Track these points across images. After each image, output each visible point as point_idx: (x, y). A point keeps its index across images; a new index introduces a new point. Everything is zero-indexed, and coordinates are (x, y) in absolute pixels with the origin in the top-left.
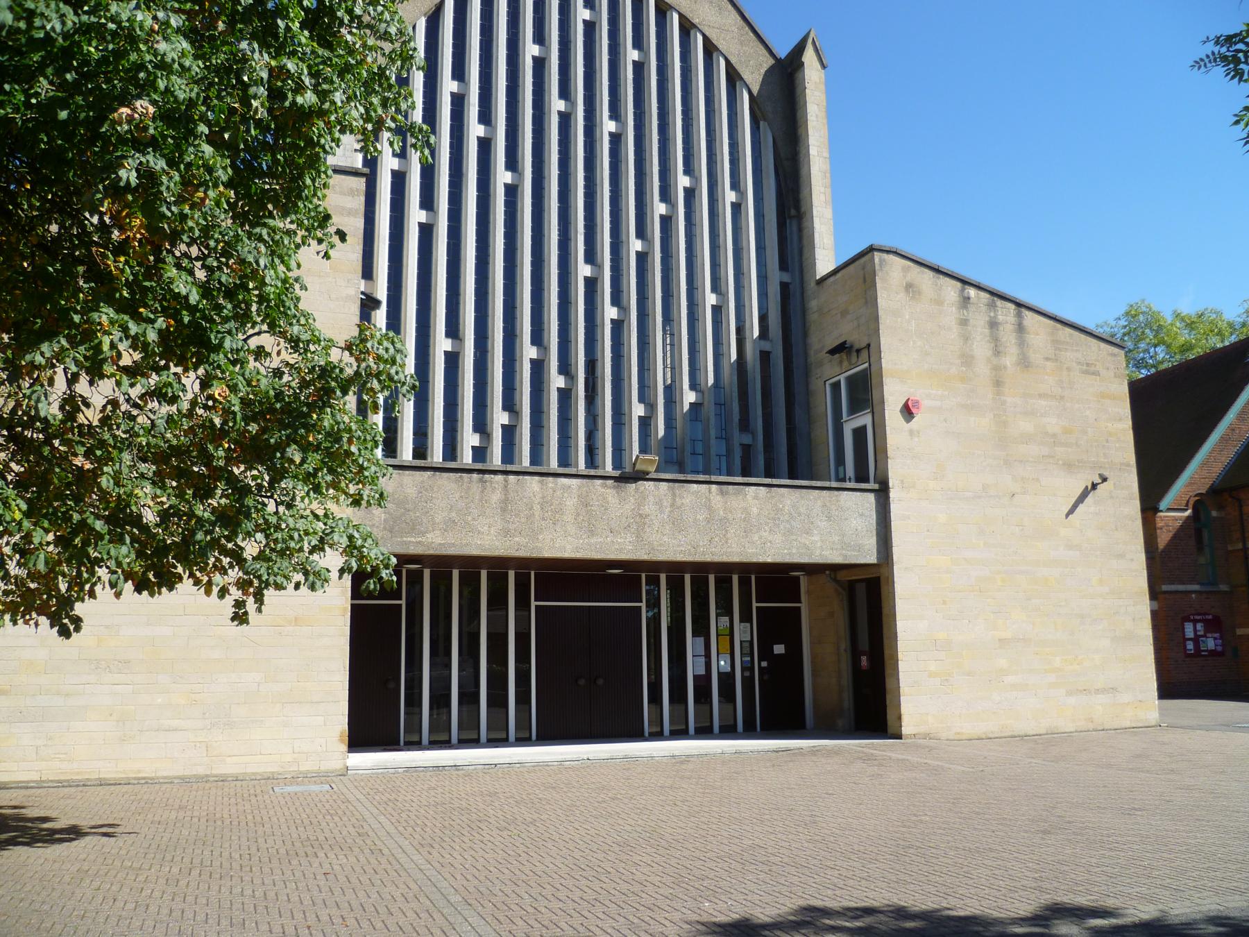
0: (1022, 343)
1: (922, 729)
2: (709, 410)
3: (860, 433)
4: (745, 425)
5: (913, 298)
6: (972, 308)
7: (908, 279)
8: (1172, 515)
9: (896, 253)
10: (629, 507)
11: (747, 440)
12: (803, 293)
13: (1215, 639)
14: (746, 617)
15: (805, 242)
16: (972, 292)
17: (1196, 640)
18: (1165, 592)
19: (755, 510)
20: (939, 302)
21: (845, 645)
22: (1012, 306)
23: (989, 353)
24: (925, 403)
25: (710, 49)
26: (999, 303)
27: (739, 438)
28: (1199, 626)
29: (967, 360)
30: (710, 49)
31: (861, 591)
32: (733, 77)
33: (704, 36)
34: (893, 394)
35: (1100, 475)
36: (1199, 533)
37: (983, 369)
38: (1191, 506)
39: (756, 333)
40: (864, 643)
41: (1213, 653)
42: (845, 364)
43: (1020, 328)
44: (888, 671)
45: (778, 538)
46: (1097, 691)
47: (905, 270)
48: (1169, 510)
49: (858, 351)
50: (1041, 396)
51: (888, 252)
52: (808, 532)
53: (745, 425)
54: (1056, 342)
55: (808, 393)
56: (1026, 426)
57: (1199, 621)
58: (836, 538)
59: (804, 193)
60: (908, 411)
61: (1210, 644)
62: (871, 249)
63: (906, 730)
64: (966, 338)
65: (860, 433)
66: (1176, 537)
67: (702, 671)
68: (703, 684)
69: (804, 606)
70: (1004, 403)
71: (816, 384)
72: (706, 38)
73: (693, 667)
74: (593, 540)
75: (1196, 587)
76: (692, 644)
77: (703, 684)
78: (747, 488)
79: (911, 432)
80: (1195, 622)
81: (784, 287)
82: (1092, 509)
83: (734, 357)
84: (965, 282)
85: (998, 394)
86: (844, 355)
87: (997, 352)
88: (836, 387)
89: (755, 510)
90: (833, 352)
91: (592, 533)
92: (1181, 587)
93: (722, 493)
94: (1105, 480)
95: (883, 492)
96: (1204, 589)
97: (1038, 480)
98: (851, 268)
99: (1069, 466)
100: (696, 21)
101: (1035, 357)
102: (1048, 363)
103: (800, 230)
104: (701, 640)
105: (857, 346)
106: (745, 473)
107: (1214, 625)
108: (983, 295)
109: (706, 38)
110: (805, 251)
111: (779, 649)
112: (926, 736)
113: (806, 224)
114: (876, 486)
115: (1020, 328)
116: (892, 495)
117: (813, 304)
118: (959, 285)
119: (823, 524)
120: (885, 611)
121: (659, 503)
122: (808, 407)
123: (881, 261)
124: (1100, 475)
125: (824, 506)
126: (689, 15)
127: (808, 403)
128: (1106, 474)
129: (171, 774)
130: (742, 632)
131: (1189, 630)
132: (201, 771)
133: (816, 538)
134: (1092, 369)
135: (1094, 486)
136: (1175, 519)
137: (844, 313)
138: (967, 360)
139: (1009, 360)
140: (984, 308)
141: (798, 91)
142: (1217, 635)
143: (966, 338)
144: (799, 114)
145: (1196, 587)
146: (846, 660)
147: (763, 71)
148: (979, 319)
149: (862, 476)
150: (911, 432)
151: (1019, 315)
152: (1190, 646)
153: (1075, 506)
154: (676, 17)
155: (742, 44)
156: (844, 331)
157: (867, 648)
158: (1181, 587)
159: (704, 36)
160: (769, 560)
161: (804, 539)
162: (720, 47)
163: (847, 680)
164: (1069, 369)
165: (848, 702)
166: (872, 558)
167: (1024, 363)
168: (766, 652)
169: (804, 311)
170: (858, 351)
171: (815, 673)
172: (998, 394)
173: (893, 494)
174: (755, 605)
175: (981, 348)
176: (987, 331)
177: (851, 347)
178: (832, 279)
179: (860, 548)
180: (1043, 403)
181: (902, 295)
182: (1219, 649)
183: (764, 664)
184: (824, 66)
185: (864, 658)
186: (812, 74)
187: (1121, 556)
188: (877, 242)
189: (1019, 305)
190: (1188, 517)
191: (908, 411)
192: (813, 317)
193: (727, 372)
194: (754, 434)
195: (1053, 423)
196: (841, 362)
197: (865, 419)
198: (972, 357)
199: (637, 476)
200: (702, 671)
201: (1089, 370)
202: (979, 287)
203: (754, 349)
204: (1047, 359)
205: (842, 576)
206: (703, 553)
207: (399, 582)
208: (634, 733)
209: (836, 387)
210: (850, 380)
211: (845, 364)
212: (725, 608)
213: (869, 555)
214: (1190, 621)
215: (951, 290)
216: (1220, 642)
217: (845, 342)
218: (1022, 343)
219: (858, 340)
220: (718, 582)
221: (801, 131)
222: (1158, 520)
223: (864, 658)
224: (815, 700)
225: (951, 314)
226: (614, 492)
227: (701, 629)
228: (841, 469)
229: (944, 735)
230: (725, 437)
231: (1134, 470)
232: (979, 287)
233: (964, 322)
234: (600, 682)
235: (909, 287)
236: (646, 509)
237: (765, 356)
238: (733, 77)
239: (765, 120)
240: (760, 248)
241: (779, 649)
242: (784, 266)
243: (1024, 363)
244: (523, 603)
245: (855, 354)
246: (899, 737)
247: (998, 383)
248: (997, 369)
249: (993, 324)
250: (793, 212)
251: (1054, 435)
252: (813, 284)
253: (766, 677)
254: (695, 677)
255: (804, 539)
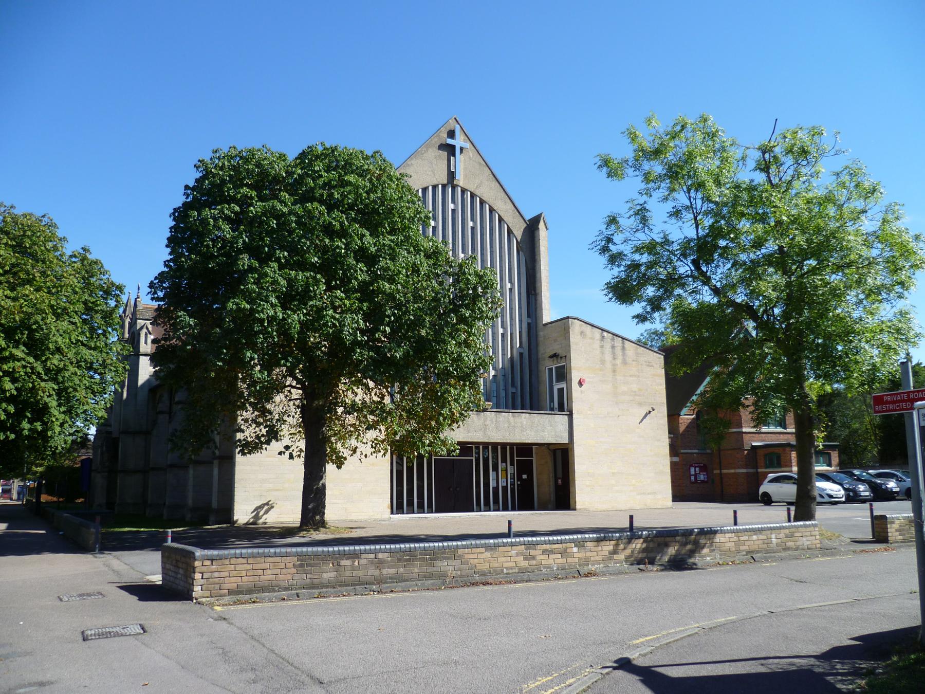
0: (624, 354)
1: (583, 507)
2: (500, 378)
3: (561, 391)
4: (513, 385)
5: (583, 338)
6: (605, 341)
7: (582, 330)
8: (686, 416)
9: (577, 319)
10: (481, 421)
11: (514, 390)
12: (536, 328)
13: (704, 475)
14: (512, 464)
15: (538, 305)
16: (605, 334)
17: (695, 475)
18: (682, 453)
19: (525, 423)
20: (593, 339)
21: (552, 475)
22: (621, 339)
23: (611, 359)
24: (587, 380)
25: (501, 220)
26: (616, 338)
27: (511, 390)
28: (697, 469)
29: (603, 362)
30: (501, 220)
31: (559, 454)
32: (510, 232)
33: (499, 215)
34: (575, 376)
35: (652, 408)
36: (698, 426)
37: (609, 366)
38: (695, 413)
39: (518, 346)
40: (560, 474)
41: (703, 482)
42: (555, 362)
43: (623, 348)
44: (571, 484)
45: (533, 433)
46: (648, 494)
47: (581, 326)
48: (685, 415)
49: (561, 358)
50: (630, 376)
51: (574, 319)
52: (543, 431)
53: (513, 385)
54: (637, 354)
55: (538, 371)
56: (624, 388)
57: (697, 467)
58: (553, 433)
59: (538, 285)
60: (580, 383)
61: (702, 477)
62: (568, 318)
63: (577, 507)
64: (603, 353)
65: (561, 391)
66: (688, 427)
67: (505, 485)
68: (496, 490)
69: (534, 459)
70: (616, 379)
71: (542, 368)
72: (499, 216)
73: (492, 484)
74: (469, 434)
75: (696, 451)
76: (492, 475)
77: (496, 490)
78: (522, 414)
79: (581, 392)
80: (695, 467)
81: (529, 324)
82: (649, 421)
83: (509, 356)
84: (603, 330)
85: (614, 375)
86: (555, 358)
87: (614, 359)
88: (551, 370)
89: (525, 423)
90: (551, 357)
91: (469, 432)
92: (690, 451)
93: (513, 416)
94: (654, 410)
95: (570, 415)
96: (700, 452)
97: (628, 410)
98: (559, 323)
99: (640, 404)
100: (495, 208)
101: (629, 360)
102: (634, 362)
103: (536, 300)
104: (495, 472)
105: (561, 355)
106: (522, 409)
107: (704, 468)
108: (610, 335)
109: (499, 216)
110: (538, 309)
111: (525, 477)
112: (585, 509)
113: (538, 298)
114: (568, 413)
115: (623, 348)
116: (574, 417)
117: (541, 334)
118: (601, 331)
119: (549, 428)
120: (570, 461)
121: (491, 420)
122: (538, 377)
123: (572, 323)
124: (652, 408)
125: (549, 421)
126: (493, 206)
127: (538, 375)
128: (654, 407)
129: (335, 519)
130: (510, 470)
131: (692, 471)
132: (344, 518)
133: (546, 433)
134: (651, 364)
135: (650, 412)
136: (688, 419)
137: (555, 341)
138: (603, 362)
139: (619, 361)
140: (610, 341)
141: (536, 239)
142: (705, 473)
143: (603, 353)
144: (536, 250)
145: (696, 451)
146: (552, 483)
147: (522, 230)
148: (608, 346)
149: (561, 408)
150: (581, 392)
151: (623, 343)
152: (693, 478)
153: (642, 420)
154: (487, 206)
155: (514, 218)
156: (555, 348)
157: (561, 476)
158: (690, 451)
159: (499, 215)
160: (530, 442)
161: (542, 434)
162: (505, 219)
163: (552, 488)
164: (641, 365)
165: (553, 497)
166: (566, 442)
167: (625, 362)
168: (520, 478)
169: (537, 336)
170: (561, 358)
171: (538, 486)
172: (614, 375)
173: (574, 416)
174: (516, 458)
175: (608, 357)
176: (611, 350)
177: (558, 355)
178: (550, 325)
179: (561, 437)
180: (631, 378)
181: (579, 336)
182: (706, 479)
183: (519, 483)
184: (547, 229)
185: (560, 480)
186: (542, 232)
187: (659, 440)
188: (570, 315)
189: (623, 339)
190: (693, 418)
191: (580, 383)
192: (541, 339)
193: (506, 361)
194: (516, 388)
195: (635, 387)
196: (553, 360)
197: (563, 385)
198: (605, 361)
199: (485, 410)
200: (505, 485)
201: (650, 365)
202: (608, 332)
203: (517, 352)
204: (633, 361)
205: (551, 447)
206: (507, 439)
207: (453, 456)
208: (472, 511)
209: (551, 370)
210: (556, 368)
211: (555, 362)
212: (504, 460)
213: (565, 440)
214: (692, 466)
215: (597, 333)
216: (706, 476)
217: (556, 353)
218: (624, 354)
219: (561, 353)
220: (483, 448)
221: (537, 257)
222: (680, 419)
223: (560, 480)
224: (538, 498)
225: (597, 343)
226: (476, 416)
227: (495, 469)
228: (552, 404)
229: (591, 510)
230: (506, 390)
231: (666, 405)
232: (608, 332)
233: (602, 347)
234: (458, 489)
235: (582, 333)
236: (487, 423)
237: (521, 354)
238: (510, 232)
239: (522, 251)
240: (520, 308)
241: (525, 477)
242: (529, 316)
243: (625, 362)
244: (478, 460)
245: (559, 359)
246: (575, 510)
247: (614, 371)
248: (614, 365)
249: (613, 347)
250: (533, 292)
251: (635, 392)
252: (541, 325)
253: (520, 488)
254: (493, 488)
255: (542, 434)
